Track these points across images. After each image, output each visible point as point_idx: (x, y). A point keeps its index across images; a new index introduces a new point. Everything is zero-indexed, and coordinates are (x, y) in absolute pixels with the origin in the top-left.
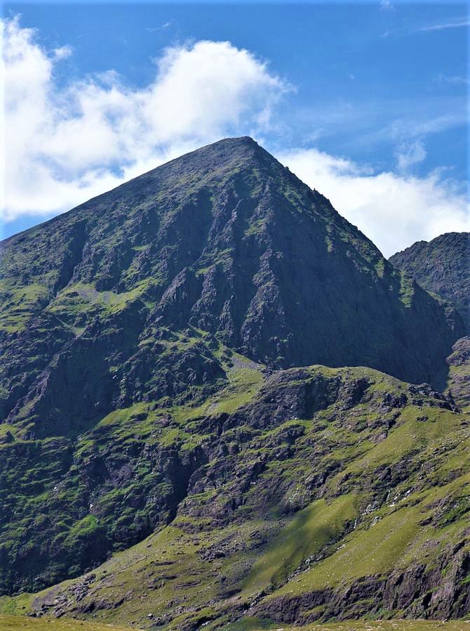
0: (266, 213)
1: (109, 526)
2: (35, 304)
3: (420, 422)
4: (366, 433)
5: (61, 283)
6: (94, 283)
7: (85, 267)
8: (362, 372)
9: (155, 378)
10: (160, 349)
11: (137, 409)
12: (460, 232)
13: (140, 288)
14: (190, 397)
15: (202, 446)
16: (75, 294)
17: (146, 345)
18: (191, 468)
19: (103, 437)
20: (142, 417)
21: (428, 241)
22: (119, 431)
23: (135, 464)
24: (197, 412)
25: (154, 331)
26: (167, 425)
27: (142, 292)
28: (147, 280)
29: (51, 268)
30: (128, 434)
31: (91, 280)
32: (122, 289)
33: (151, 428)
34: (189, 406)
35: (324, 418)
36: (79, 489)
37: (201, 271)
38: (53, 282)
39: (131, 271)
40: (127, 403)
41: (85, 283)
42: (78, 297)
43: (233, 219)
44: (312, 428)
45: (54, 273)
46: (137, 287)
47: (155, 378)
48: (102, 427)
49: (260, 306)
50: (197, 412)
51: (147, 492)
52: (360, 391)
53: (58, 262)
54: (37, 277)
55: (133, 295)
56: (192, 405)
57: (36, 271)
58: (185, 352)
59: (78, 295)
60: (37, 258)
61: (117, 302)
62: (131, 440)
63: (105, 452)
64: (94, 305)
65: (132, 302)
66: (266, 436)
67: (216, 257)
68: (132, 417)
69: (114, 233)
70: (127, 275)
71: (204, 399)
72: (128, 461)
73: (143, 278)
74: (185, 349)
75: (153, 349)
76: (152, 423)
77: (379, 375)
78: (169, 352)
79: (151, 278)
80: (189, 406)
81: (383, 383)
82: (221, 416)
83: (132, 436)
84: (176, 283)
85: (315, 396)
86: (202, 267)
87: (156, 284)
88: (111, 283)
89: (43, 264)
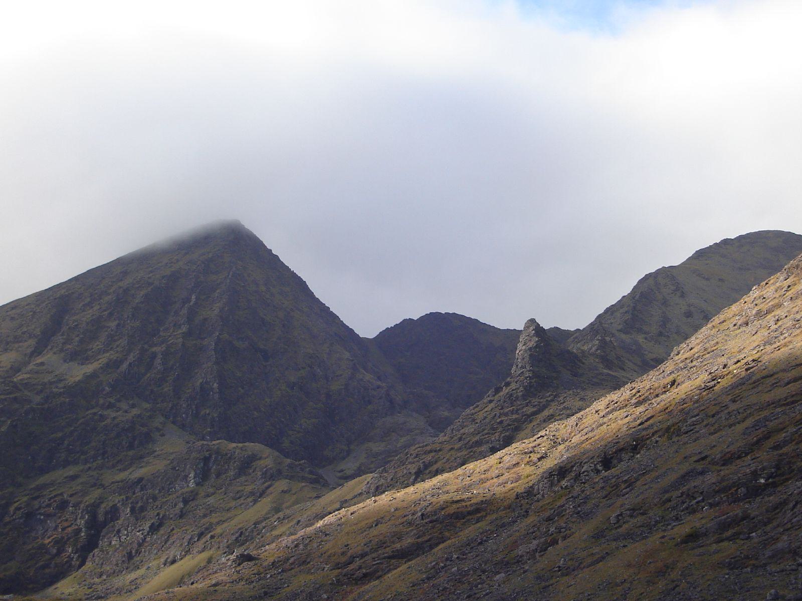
0: (221, 298)
1: (28, 570)
2: (7, 371)
3: (282, 493)
4: (242, 500)
5: (37, 351)
6: (62, 355)
7: (59, 339)
8: (253, 447)
9: (94, 444)
10: (102, 418)
11: (71, 471)
12: (593, 320)
13: (100, 361)
14: (119, 461)
15: (118, 505)
16: (42, 364)
17: (91, 414)
18: (105, 524)
19: (36, 494)
20: (73, 478)
21: (581, 329)
22: (51, 489)
23: (60, 517)
24: (123, 475)
25: (101, 401)
26: (94, 485)
27: (101, 365)
28: (108, 354)
29: (30, 337)
30: (59, 492)
31: (61, 351)
32: (86, 360)
33: (79, 488)
34: (117, 470)
35: (215, 486)
36: (8, 538)
37: (154, 349)
38: (29, 351)
39: (97, 345)
40: (66, 464)
41: (55, 353)
42: (44, 367)
43: (191, 303)
44: (203, 494)
45: (32, 342)
46: (98, 360)
47: (94, 444)
48: (38, 485)
49: (198, 384)
50: (123, 475)
51: (65, 543)
52: (247, 465)
53: (38, 332)
54: (16, 345)
55: (89, 369)
56: (120, 469)
57: (17, 339)
58: (123, 422)
59: (44, 365)
60: (21, 326)
61: (77, 373)
62: (60, 497)
63: (37, 507)
64: (56, 376)
65: (89, 374)
66: (166, 499)
67: (170, 336)
68: (66, 478)
69: (92, 307)
70: (92, 349)
71: (131, 465)
72: (55, 515)
73: (105, 351)
74: (123, 420)
75: (96, 417)
76: (82, 483)
77: (267, 451)
78: (109, 421)
79: (112, 352)
80: (117, 470)
81: (268, 458)
82: (138, 480)
83: (62, 494)
84: (131, 358)
85: (212, 467)
86: (156, 345)
87: (115, 358)
88: (78, 356)
89: (24, 333)
